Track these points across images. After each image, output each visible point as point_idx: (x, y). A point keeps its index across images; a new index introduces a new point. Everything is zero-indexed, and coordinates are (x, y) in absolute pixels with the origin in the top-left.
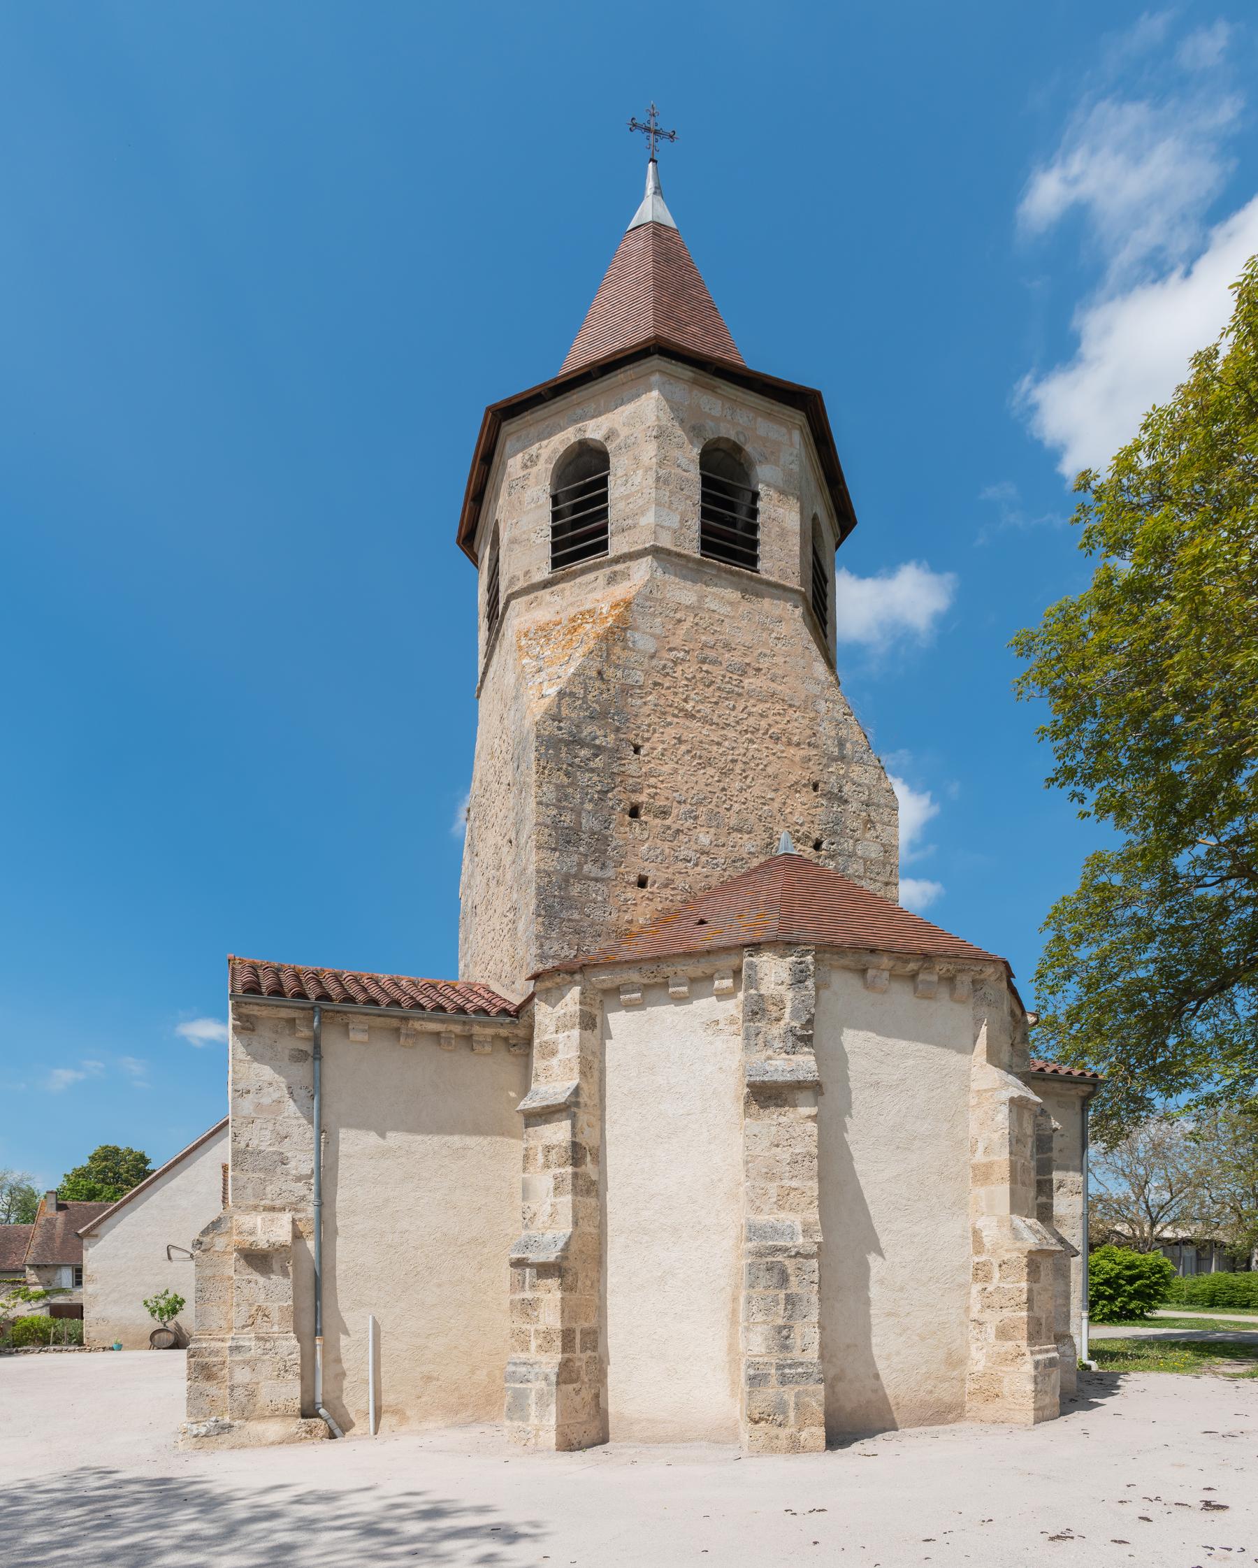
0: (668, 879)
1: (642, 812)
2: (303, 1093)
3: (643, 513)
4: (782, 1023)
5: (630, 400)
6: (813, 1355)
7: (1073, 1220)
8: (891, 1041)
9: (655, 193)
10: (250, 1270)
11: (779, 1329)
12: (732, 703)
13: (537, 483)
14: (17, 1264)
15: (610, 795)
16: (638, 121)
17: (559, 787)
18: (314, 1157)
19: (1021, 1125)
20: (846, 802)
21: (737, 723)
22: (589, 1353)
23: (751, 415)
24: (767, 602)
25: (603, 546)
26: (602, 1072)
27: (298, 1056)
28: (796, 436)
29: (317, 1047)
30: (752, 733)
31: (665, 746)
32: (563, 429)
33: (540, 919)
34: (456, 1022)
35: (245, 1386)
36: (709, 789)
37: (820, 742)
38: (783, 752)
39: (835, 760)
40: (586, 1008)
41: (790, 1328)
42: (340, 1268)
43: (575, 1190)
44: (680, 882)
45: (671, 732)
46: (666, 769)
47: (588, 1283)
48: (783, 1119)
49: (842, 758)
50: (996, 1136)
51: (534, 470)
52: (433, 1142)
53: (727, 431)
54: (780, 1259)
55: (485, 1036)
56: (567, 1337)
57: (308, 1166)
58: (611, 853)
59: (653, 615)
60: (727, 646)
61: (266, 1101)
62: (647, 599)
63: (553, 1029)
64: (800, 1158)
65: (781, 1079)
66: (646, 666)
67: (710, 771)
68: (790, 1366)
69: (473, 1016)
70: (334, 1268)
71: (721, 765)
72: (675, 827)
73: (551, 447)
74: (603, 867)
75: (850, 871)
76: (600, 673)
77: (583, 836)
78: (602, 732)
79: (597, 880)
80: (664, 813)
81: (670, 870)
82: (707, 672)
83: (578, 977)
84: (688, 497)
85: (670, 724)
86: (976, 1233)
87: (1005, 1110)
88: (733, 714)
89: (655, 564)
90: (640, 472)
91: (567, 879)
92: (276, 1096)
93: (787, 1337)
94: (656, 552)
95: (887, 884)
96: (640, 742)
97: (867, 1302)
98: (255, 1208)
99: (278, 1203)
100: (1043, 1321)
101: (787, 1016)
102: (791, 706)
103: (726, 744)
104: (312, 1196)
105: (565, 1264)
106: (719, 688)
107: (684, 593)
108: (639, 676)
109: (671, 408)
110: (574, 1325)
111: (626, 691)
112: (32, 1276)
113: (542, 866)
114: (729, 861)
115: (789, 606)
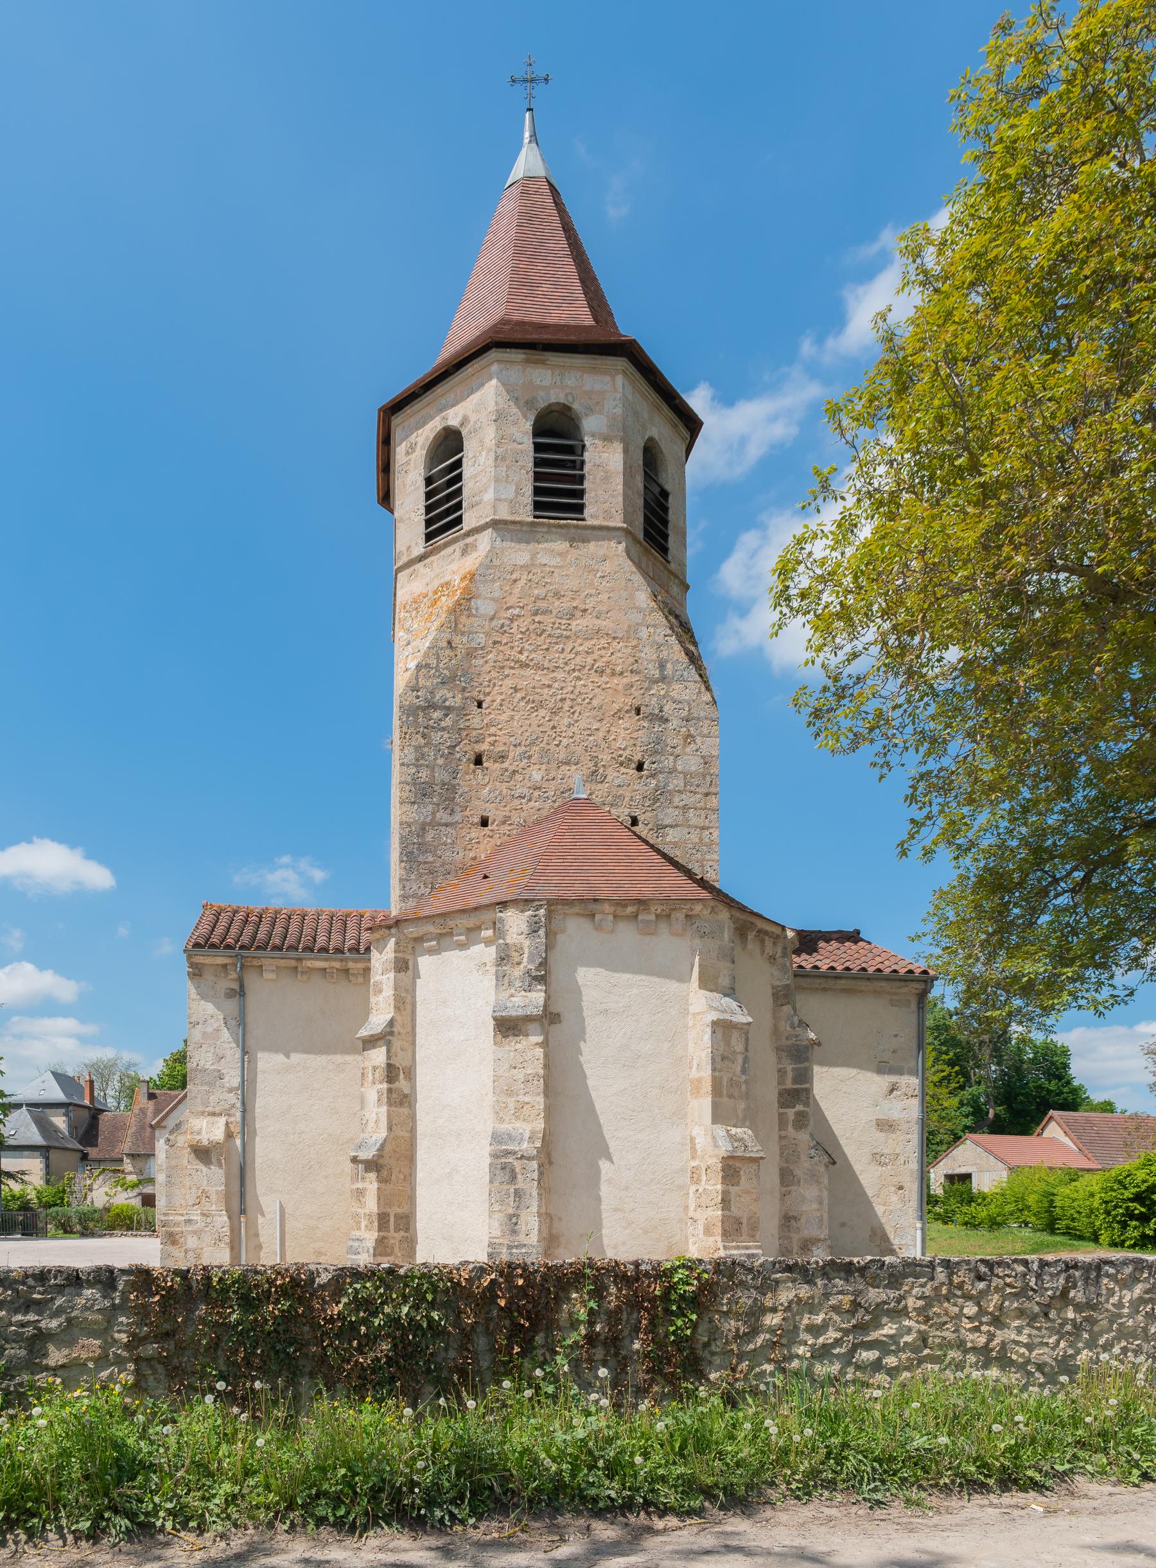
0: (505, 816)
1: (484, 759)
2: (234, 1022)
3: (486, 491)
4: (522, 966)
5: (478, 389)
6: (534, 1239)
7: (907, 1125)
8: (617, 975)
9: (530, 142)
10: (197, 1162)
11: (511, 1217)
12: (561, 646)
13: (415, 468)
14: (114, 1155)
15: (457, 749)
16: (517, 76)
17: (418, 748)
18: (239, 1072)
19: (728, 1043)
20: (667, 720)
21: (566, 664)
22: (402, 1233)
23: (579, 374)
24: (592, 546)
25: (459, 521)
26: (414, 1005)
27: (231, 993)
28: (620, 379)
29: (242, 986)
30: (579, 670)
31: (503, 697)
32: (433, 418)
33: (403, 864)
34: (335, 960)
35: (194, 1250)
36: (541, 729)
37: (641, 668)
38: (607, 683)
39: (656, 682)
40: (400, 955)
41: (518, 1216)
42: (258, 1161)
43: (390, 1103)
44: (515, 818)
45: (509, 682)
46: (504, 717)
47: (402, 1177)
48: (519, 1046)
49: (663, 679)
50: (704, 1054)
51: (413, 456)
52: (322, 1060)
53: (557, 396)
54: (510, 1160)
55: (358, 969)
56: (383, 1220)
57: (236, 1082)
58: (458, 800)
59: (493, 581)
60: (558, 595)
61: (209, 1030)
62: (488, 567)
63: (380, 971)
64: (530, 1078)
65: (514, 1014)
66: (487, 628)
67: (542, 712)
68: (517, 1247)
69: (348, 954)
70: (254, 1160)
71: (551, 705)
72: (511, 768)
73: (424, 436)
74: (452, 812)
75: (671, 787)
76: (449, 643)
77: (436, 788)
78: (451, 694)
79: (446, 825)
80: (503, 757)
81: (507, 808)
82: (539, 622)
83: (393, 931)
84: (523, 467)
85: (508, 676)
86: (692, 1140)
87: (709, 1030)
88: (562, 656)
89: (495, 535)
90: (484, 453)
91: (423, 828)
92: (215, 1026)
93: (516, 1224)
94: (495, 524)
95: (707, 795)
96: (482, 697)
97: (599, 1199)
98: (203, 1113)
99: (217, 1110)
100: (744, 1221)
101: (525, 960)
102: (614, 638)
103: (556, 685)
104: (239, 1105)
105: (381, 1161)
106: (549, 635)
107: (519, 554)
108: (481, 639)
109: (508, 391)
110: (388, 1210)
111: (470, 654)
112: (128, 1165)
113: (405, 819)
114: (558, 793)
115: (613, 544)
